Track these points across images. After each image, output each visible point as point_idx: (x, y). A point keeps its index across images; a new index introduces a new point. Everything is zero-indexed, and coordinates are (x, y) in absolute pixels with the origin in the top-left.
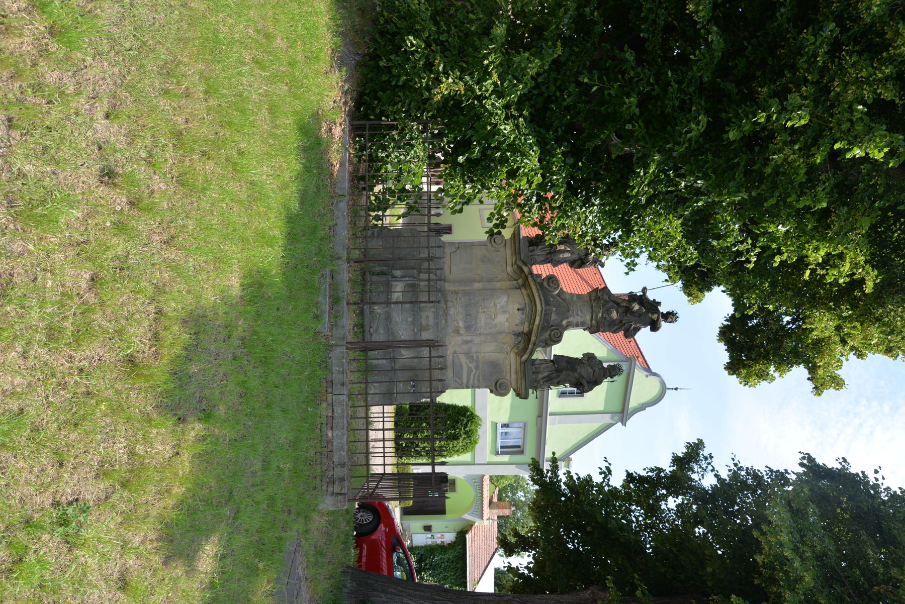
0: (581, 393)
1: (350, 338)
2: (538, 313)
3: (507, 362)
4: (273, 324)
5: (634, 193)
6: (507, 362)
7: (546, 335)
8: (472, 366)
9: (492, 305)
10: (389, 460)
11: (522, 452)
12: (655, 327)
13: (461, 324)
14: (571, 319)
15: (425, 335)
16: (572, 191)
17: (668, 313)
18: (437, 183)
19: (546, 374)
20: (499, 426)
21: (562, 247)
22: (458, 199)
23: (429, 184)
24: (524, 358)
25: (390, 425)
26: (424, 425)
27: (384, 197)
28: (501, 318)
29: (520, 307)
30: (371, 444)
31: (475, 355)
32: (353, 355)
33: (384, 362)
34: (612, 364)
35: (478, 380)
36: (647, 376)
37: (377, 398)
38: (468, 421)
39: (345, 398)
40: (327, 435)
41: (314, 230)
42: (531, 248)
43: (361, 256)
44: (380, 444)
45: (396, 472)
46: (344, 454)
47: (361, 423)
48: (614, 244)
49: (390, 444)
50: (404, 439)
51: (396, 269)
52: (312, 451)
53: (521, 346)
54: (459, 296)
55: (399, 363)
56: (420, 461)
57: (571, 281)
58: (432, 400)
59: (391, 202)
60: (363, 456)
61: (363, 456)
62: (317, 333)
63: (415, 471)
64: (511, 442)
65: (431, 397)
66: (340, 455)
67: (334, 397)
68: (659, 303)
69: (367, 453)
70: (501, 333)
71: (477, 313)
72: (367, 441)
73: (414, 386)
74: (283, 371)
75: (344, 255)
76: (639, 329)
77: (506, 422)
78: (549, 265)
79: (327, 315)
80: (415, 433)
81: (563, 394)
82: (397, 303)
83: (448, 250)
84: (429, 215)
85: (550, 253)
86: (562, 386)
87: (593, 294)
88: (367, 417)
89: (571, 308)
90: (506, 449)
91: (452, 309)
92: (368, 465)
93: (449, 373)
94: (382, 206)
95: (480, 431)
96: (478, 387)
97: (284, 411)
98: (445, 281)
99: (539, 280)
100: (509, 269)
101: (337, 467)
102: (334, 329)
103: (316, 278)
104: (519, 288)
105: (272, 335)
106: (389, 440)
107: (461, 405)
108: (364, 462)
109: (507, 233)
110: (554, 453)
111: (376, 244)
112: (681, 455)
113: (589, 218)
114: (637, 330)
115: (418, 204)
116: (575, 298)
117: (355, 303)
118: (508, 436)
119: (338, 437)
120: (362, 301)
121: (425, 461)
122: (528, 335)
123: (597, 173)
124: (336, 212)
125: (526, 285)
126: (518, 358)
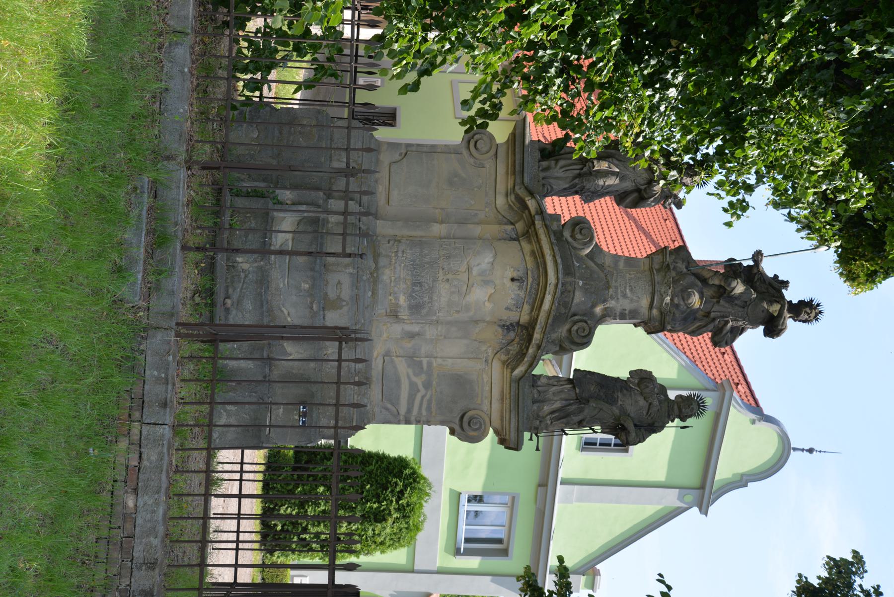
0: (624, 445)
1: (185, 314)
2: (550, 288)
3: (486, 378)
4: (24, 280)
5: (754, 63)
6: (486, 378)
7: (562, 331)
8: (419, 381)
9: (464, 268)
10: (246, 557)
11: (505, 553)
12: (773, 329)
13: (402, 300)
14: (611, 304)
15: (333, 319)
16: (631, 53)
17: (801, 302)
18: (373, 25)
19: (557, 405)
20: (464, 498)
21: (604, 165)
22: (410, 59)
23: (357, 24)
24: (518, 371)
25: (256, 488)
26: (321, 489)
27: (267, 44)
28: (479, 295)
29: (515, 275)
30: (214, 524)
31: (425, 361)
32: (189, 348)
33: (250, 364)
34: (685, 393)
35: (429, 408)
36: (753, 422)
37: (231, 434)
38: (405, 486)
39: (167, 431)
40: (125, 504)
41: (122, 96)
42: (545, 164)
43: (216, 157)
44: (232, 525)
45: (258, 580)
46: (156, 542)
47: (196, 482)
48: (705, 164)
49: (254, 525)
50: (280, 517)
51: (285, 188)
52: (90, 535)
53: (514, 348)
54: (402, 247)
55: (280, 369)
56: (307, 560)
57: (616, 231)
58: (338, 442)
59: (279, 56)
60: (195, 547)
61: (195, 547)
62: (118, 301)
63: (297, 581)
64: (485, 532)
65: (335, 437)
66: (148, 544)
67: (145, 429)
68: (785, 284)
69: (204, 543)
70: (476, 322)
71: (435, 280)
72: (206, 518)
73: (304, 415)
74: (41, 375)
75: (181, 152)
76: (742, 331)
77: (477, 490)
78: (577, 197)
79: (140, 267)
80: (302, 505)
81: (588, 445)
82: (281, 252)
83: (386, 158)
84: (354, 86)
85: (579, 176)
86: (587, 430)
87: (658, 259)
88: (208, 471)
89: (613, 284)
90: (476, 545)
91: (387, 272)
92: (203, 565)
93: (375, 392)
94: (264, 62)
95: (427, 507)
96: (429, 423)
97: (37, 453)
98: (376, 216)
99: (555, 226)
100: (501, 201)
101: (139, 568)
102: (154, 297)
103: (121, 193)
104: (517, 239)
105: (22, 301)
106: (250, 517)
107: (393, 453)
108: (195, 560)
109: (499, 130)
110: (561, 559)
111: (244, 135)
112: (815, 582)
113: (653, 115)
114: (738, 332)
115: (335, 63)
116: (621, 264)
117: (198, 249)
118: (478, 520)
119: (147, 508)
120: (213, 245)
121: (317, 561)
122: (528, 329)
123: (683, 24)
124: (167, 65)
125: (530, 234)
126: (507, 372)
